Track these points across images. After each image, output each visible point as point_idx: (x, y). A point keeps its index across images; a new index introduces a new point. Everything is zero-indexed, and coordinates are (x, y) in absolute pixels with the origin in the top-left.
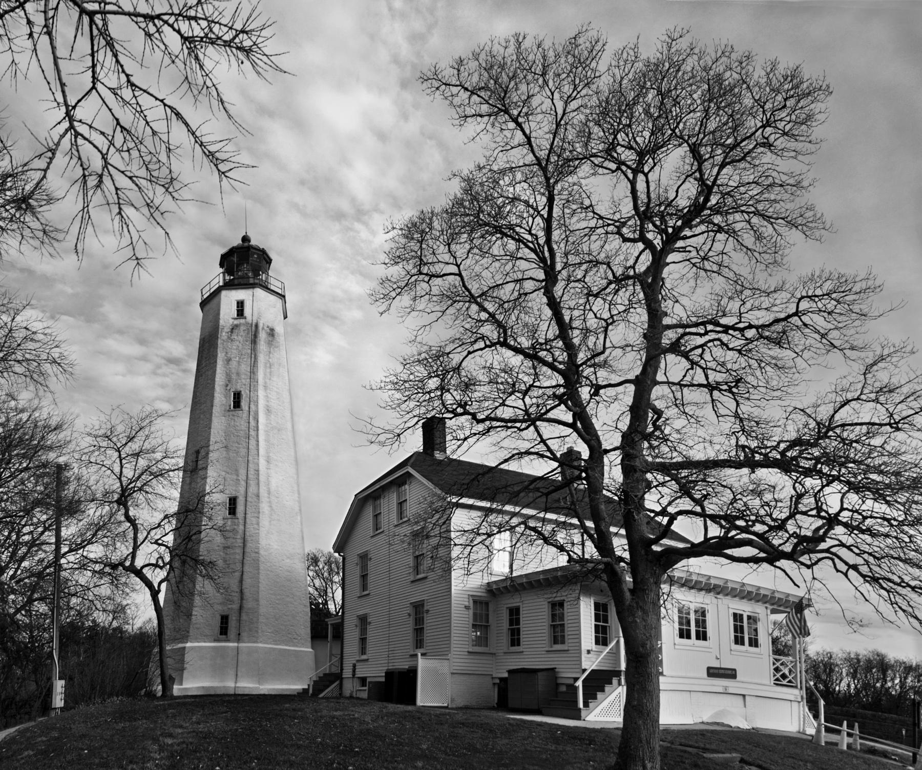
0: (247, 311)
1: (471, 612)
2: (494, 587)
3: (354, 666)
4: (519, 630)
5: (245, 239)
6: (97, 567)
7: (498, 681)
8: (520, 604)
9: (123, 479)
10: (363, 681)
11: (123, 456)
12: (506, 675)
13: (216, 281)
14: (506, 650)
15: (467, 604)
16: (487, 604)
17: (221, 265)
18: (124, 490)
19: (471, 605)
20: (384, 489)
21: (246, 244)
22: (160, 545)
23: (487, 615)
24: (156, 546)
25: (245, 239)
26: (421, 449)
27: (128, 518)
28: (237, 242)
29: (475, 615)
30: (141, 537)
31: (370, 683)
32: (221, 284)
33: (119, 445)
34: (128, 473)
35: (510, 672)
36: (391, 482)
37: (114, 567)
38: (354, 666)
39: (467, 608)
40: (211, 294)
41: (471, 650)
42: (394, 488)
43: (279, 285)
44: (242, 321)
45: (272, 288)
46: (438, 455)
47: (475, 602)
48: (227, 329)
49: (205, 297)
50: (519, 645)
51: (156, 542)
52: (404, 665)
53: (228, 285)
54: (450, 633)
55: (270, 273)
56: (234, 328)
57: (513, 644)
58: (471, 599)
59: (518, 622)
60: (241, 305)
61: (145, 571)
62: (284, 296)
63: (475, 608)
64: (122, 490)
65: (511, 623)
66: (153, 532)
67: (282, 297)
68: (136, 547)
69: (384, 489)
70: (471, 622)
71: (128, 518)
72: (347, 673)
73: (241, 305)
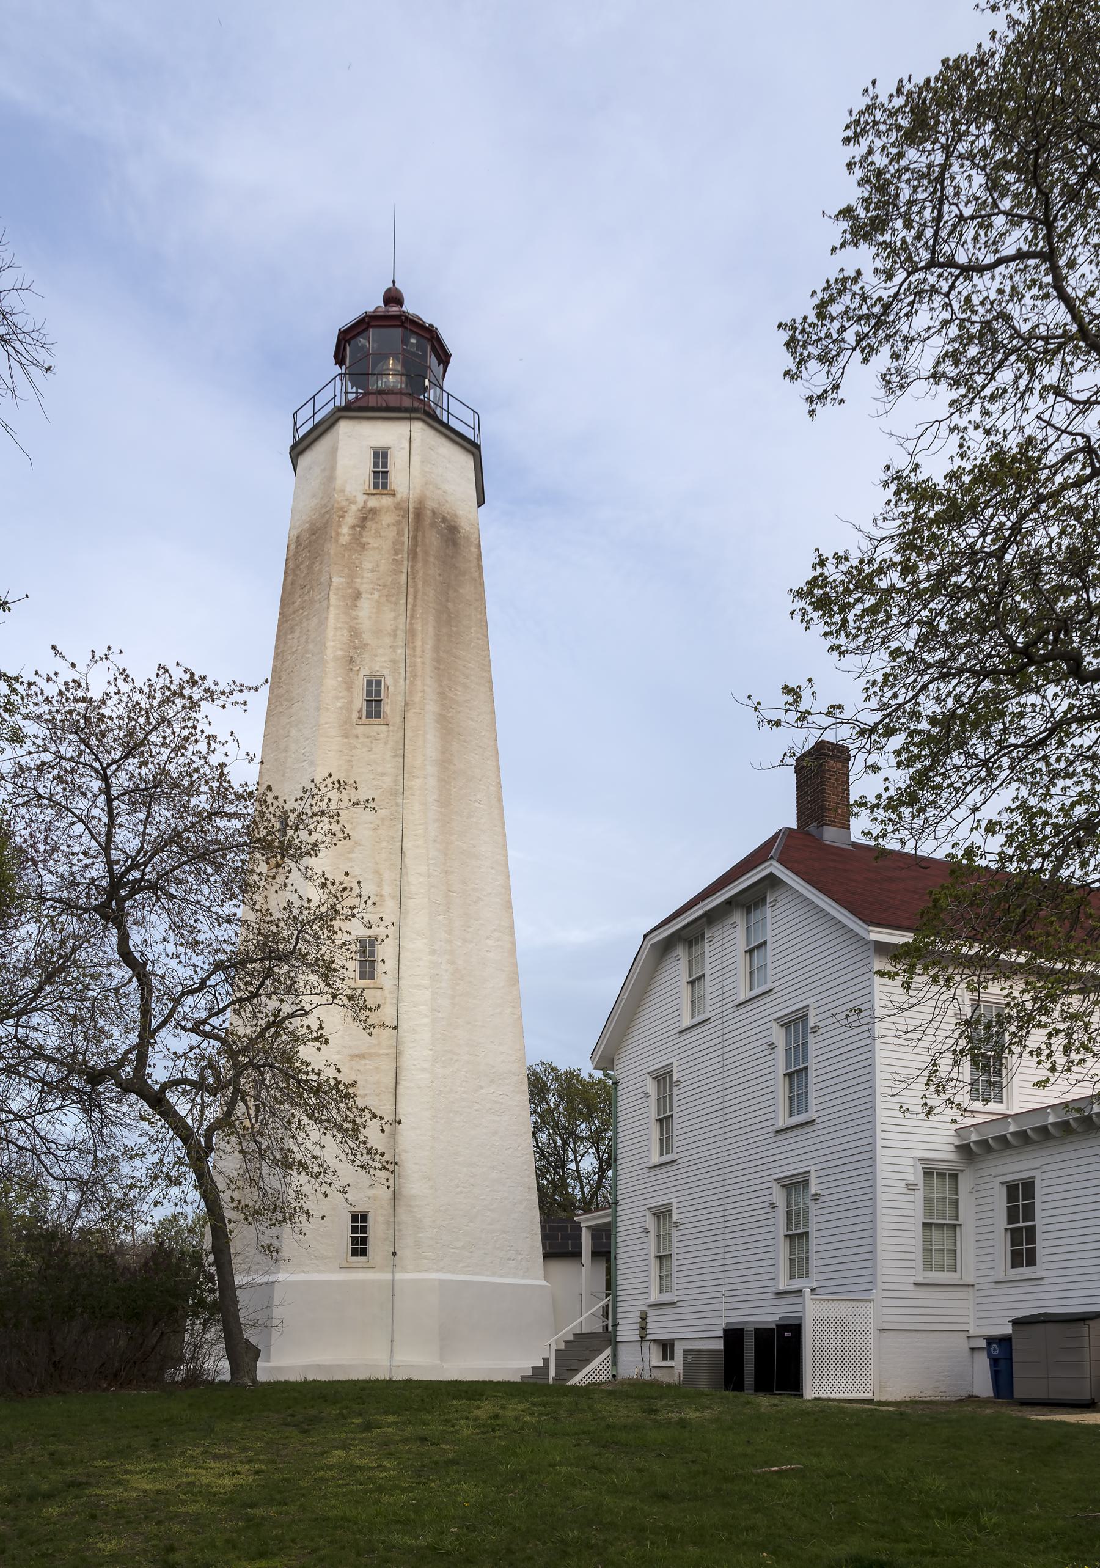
0: (397, 479)
1: (920, 1195)
2: (974, 1137)
3: (644, 1318)
4: (1031, 1231)
5: (393, 297)
6: (54, 1072)
7: (983, 1344)
8: (1035, 1173)
9: (115, 855)
10: (667, 1348)
11: (114, 792)
12: (1008, 1330)
13: (328, 393)
14: (1001, 1276)
15: (911, 1178)
16: (954, 1177)
17: (339, 359)
18: (116, 882)
19: (920, 1180)
20: (712, 918)
21: (394, 309)
22: (206, 1035)
23: (956, 1202)
24: (195, 1039)
25: (393, 297)
26: (794, 825)
27: (126, 956)
28: (374, 302)
29: (928, 1200)
30: (158, 1010)
31: (686, 1352)
32: (340, 402)
33: (105, 759)
34: (127, 840)
35: (1015, 1323)
36: (729, 902)
37: (96, 1077)
38: (644, 1318)
39: (911, 1187)
40: (315, 427)
41: (920, 1280)
42: (738, 918)
43: (468, 417)
44: (386, 501)
45: (454, 423)
46: (830, 835)
47: (928, 1174)
48: (350, 519)
49: (302, 432)
50: (1032, 1262)
51: (196, 1029)
52: (769, 1314)
53: (350, 410)
54: (874, 1244)
55: (447, 384)
56: (367, 516)
57: (1016, 1261)
58: (919, 1167)
59: (1029, 1212)
60: (381, 457)
61: (172, 1097)
62: (478, 447)
63: (928, 1188)
64: (111, 883)
65: (1012, 1216)
66: (190, 1000)
67: (472, 447)
68: (147, 1036)
69: (712, 918)
70: (920, 1219)
71: (126, 956)
72: (627, 1330)
73: (381, 457)
